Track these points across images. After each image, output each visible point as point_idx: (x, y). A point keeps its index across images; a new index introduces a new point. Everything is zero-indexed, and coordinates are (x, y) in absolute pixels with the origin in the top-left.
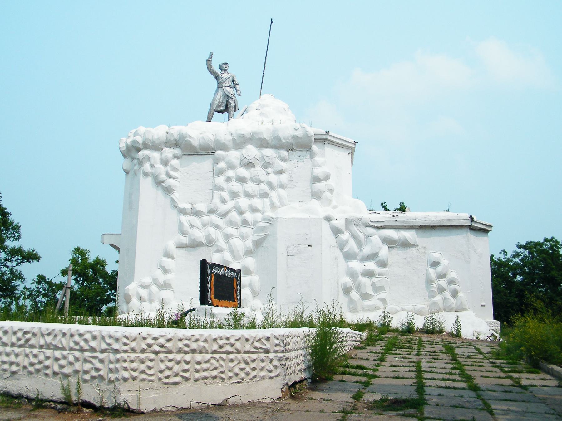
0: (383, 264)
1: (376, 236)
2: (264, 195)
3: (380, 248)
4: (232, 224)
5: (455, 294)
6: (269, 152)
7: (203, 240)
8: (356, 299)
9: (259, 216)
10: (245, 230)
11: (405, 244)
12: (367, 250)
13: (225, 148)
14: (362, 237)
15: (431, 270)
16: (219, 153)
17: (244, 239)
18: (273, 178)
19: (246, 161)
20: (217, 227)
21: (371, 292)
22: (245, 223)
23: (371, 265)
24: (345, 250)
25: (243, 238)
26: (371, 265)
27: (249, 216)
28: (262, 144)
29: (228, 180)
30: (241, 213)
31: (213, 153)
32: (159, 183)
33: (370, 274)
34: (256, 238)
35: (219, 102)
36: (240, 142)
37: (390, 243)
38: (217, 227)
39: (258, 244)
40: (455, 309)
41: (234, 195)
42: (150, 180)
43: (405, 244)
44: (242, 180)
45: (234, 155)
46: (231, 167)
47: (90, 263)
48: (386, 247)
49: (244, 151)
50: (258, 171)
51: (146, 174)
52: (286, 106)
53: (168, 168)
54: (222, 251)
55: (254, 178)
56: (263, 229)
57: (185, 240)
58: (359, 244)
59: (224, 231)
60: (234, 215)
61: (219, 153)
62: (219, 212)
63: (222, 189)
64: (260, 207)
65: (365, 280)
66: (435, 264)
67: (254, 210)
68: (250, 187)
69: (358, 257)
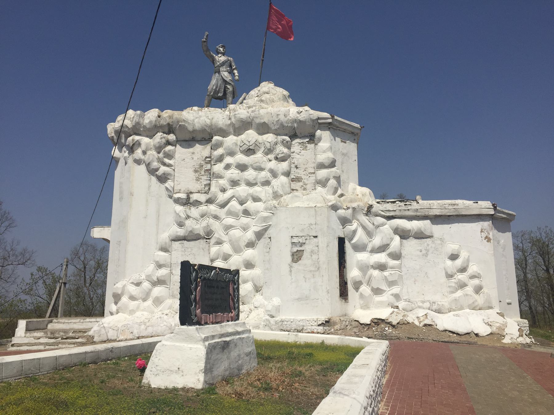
0: (396, 256)
1: (386, 226)
2: (267, 183)
3: (392, 239)
4: (230, 213)
5: (478, 290)
6: (270, 138)
7: (202, 233)
8: (367, 295)
9: (259, 206)
10: (244, 220)
11: (420, 236)
12: (377, 241)
13: (224, 133)
14: (370, 226)
15: (449, 263)
16: (216, 138)
17: (244, 230)
18: (273, 165)
19: (245, 147)
20: (216, 217)
21: (384, 287)
22: (246, 213)
23: (382, 258)
24: (353, 241)
25: (245, 229)
26: (382, 258)
27: (250, 205)
28: (263, 128)
29: (228, 167)
30: (242, 203)
31: (210, 139)
32: (152, 172)
33: (382, 267)
34: (257, 229)
35: (216, 87)
36: (242, 126)
37: (404, 235)
38: (216, 217)
39: (259, 235)
40: (478, 308)
41: (235, 183)
42: (143, 167)
43: (420, 236)
44: (242, 168)
45: (231, 140)
46: (232, 154)
47: (151, 390)
48: (397, 238)
49: (243, 137)
50: (259, 156)
51: (138, 162)
52: (286, 93)
53: (161, 155)
54: (221, 243)
55: (254, 165)
56: (265, 219)
57: (181, 232)
58: (370, 234)
59: (223, 222)
60: (234, 204)
61: (216, 138)
62: (217, 201)
63: (221, 177)
64: (262, 196)
65: (376, 273)
66: (454, 257)
67: (256, 199)
68: (250, 174)
69: (369, 248)
